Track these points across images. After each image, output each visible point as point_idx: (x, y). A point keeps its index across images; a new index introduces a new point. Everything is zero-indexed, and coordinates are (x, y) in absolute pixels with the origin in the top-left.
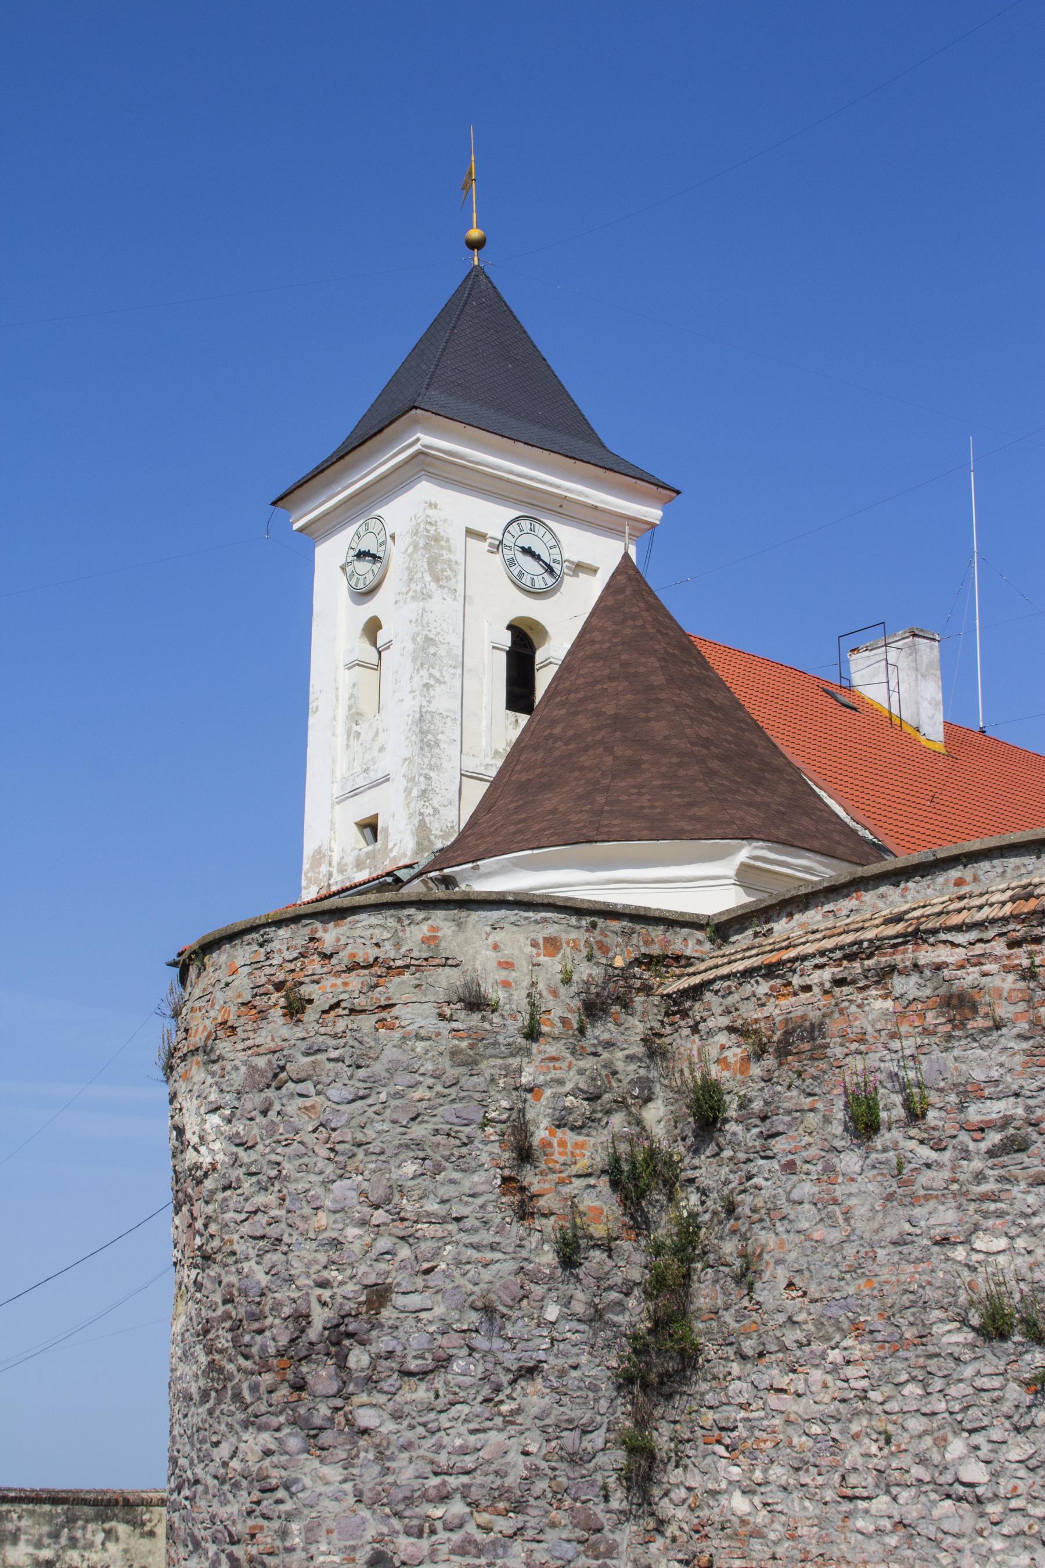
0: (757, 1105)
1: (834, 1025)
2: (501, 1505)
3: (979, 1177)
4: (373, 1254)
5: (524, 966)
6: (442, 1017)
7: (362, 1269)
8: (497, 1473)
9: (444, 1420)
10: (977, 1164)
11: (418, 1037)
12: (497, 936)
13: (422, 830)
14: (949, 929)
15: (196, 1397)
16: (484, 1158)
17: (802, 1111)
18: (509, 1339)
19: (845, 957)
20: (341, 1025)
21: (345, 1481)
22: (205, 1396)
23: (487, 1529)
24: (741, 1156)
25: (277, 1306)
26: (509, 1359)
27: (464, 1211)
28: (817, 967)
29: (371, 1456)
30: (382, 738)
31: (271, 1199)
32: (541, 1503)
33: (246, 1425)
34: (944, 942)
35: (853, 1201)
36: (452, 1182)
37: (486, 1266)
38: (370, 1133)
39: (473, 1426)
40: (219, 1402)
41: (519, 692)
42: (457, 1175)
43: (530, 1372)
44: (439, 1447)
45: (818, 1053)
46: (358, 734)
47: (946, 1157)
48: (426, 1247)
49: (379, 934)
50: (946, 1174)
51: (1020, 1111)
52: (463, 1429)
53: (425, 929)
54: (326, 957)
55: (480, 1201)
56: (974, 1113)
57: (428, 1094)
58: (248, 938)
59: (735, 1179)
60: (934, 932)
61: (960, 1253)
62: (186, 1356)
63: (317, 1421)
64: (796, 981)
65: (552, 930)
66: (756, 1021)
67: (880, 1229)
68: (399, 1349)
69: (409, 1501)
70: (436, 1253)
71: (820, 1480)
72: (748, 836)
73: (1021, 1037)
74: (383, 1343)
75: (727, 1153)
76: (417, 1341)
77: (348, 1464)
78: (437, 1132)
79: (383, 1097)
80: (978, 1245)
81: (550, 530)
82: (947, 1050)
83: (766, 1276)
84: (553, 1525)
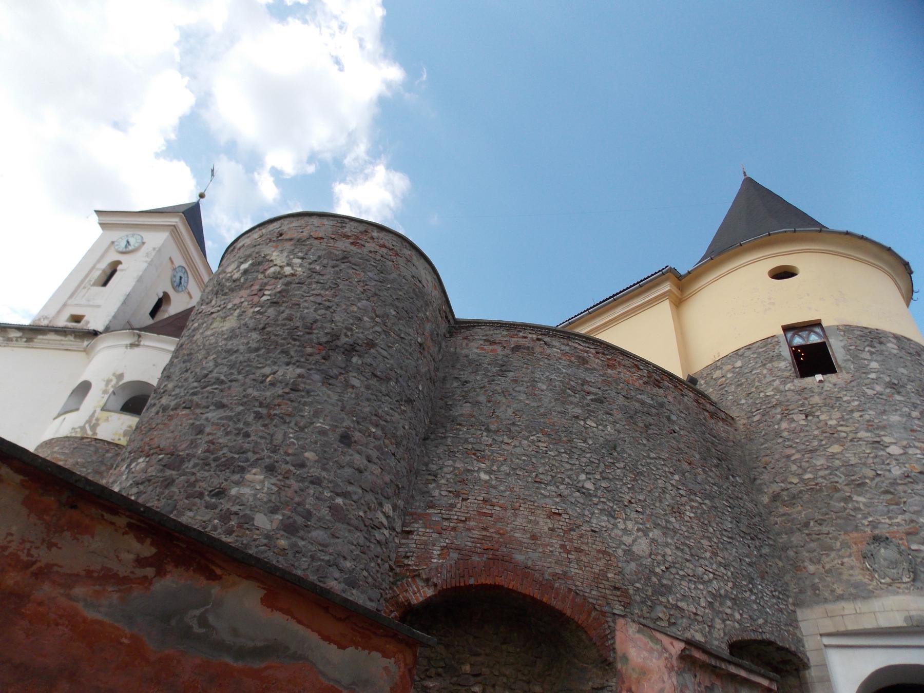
33: (288, 364)
41: (153, 313)
44: (380, 407)
49: (394, 243)
70: (394, 344)
76: (382, 366)
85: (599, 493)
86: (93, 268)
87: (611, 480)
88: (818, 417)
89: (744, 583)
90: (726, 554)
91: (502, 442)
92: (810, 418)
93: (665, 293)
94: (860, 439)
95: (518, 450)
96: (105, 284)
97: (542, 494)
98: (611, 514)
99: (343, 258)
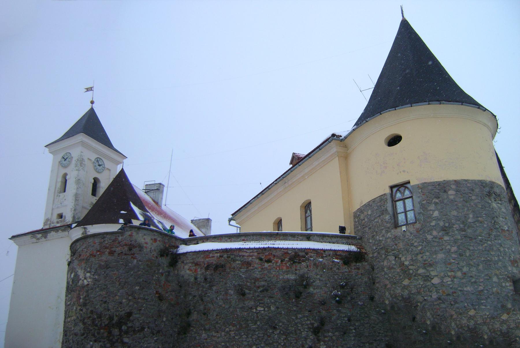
1: (228, 265)
13: (74, 217)
20: (123, 257)
24: (204, 289)
41: (94, 193)
45: (225, 271)
46: (59, 196)
58: (98, 236)
63: (114, 340)
67: (238, 305)
74: (130, 325)
76: (137, 324)
78: (143, 281)
79: (132, 273)
80: (258, 309)
83: (211, 313)
88: (400, 258)
92: (397, 259)
93: (333, 154)
94: (420, 275)
95: (220, 339)
96: (65, 191)
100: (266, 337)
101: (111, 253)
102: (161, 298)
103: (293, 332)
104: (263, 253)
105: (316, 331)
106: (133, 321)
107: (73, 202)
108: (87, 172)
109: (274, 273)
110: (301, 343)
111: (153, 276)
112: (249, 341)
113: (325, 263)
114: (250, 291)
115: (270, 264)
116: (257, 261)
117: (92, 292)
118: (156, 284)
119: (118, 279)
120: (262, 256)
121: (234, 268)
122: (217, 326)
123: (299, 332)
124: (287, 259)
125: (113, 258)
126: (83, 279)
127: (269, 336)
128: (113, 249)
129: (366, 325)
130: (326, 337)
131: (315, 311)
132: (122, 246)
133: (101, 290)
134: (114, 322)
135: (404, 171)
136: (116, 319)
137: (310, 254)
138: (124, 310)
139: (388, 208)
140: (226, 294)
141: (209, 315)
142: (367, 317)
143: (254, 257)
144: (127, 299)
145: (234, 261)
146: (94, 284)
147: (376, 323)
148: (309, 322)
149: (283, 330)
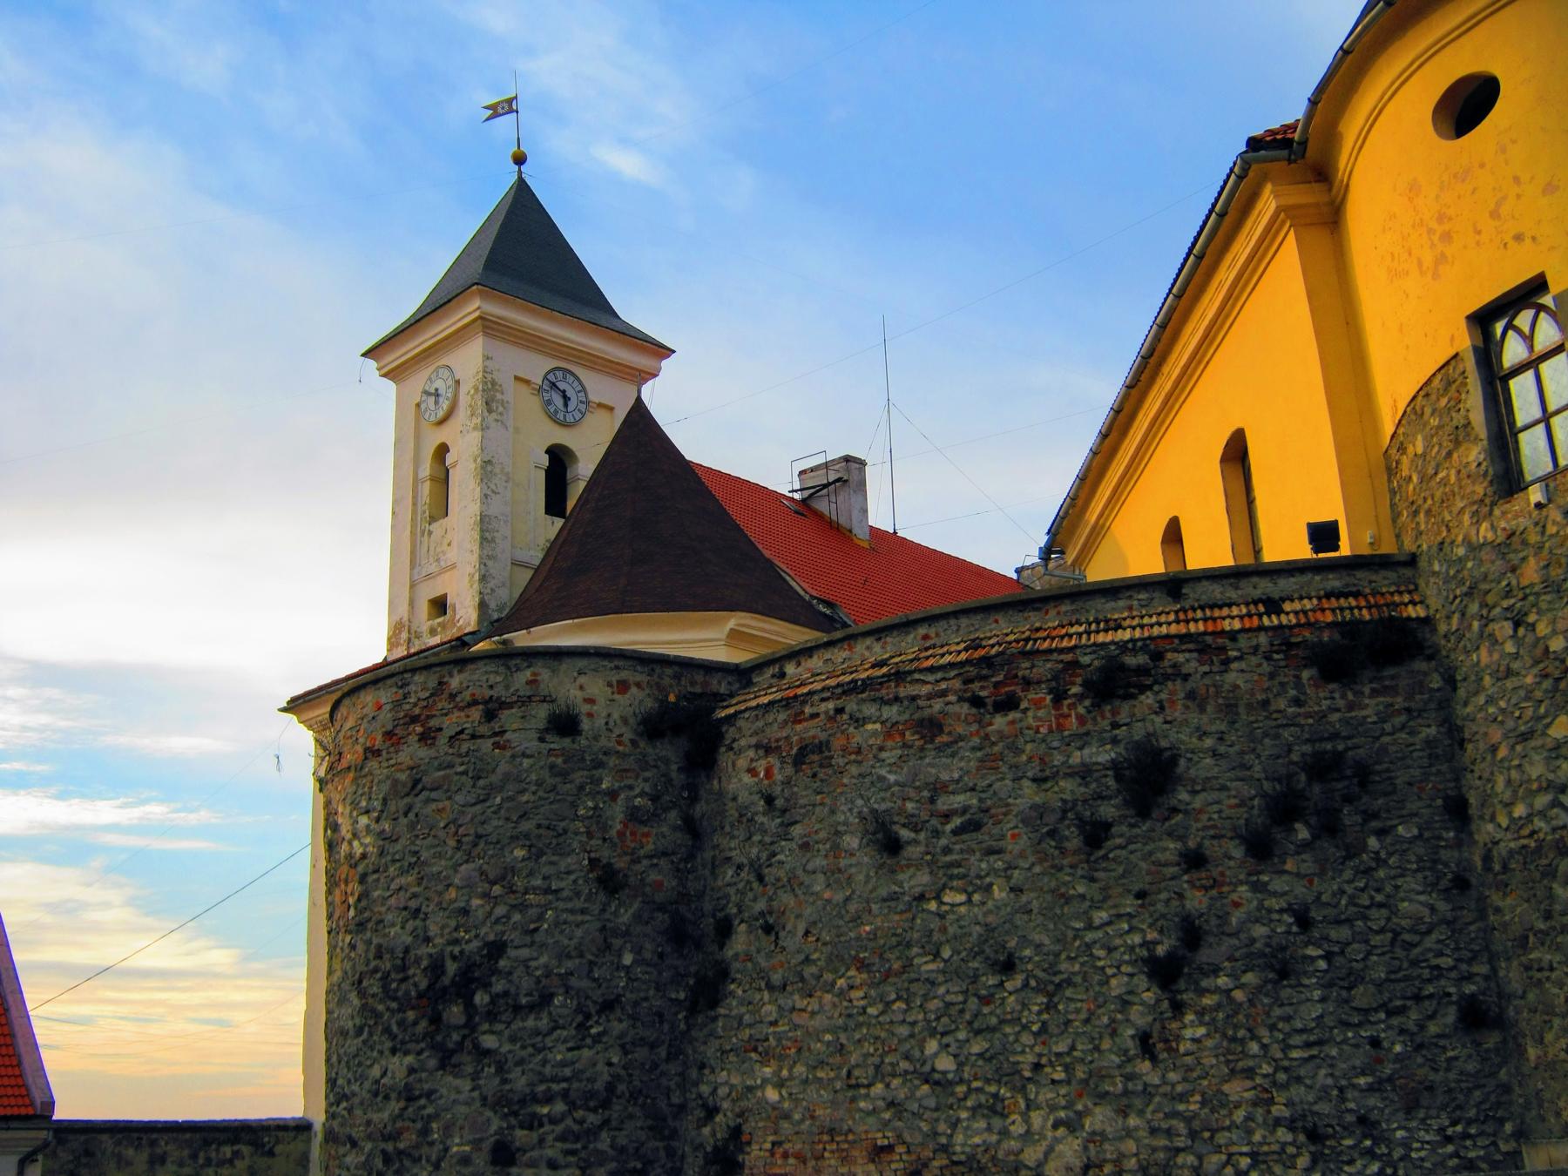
0: (779, 803)
1: (838, 742)
2: (592, 1104)
3: (947, 850)
4: (493, 918)
5: (601, 701)
6: (542, 740)
7: (483, 931)
8: (588, 1080)
9: (549, 1042)
10: (943, 842)
11: (524, 755)
12: (582, 680)
13: (483, 606)
14: (921, 671)
15: (351, 1033)
16: (575, 845)
17: (814, 805)
18: (595, 980)
19: (844, 693)
21: (473, 1090)
22: (359, 1031)
23: (581, 1122)
24: (768, 839)
25: (418, 961)
26: (597, 995)
27: (562, 884)
28: (823, 700)
29: (492, 1070)
30: (449, 536)
31: (410, 879)
32: (623, 1101)
33: (394, 1051)
34: (917, 681)
35: (853, 870)
36: (552, 863)
37: (577, 926)
38: (488, 828)
39: (570, 1045)
40: (371, 1034)
41: (555, 504)
42: (555, 858)
43: (608, 1006)
44: (545, 1062)
45: (826, 763)
47: (922, 836)
48: (533, 912)
49: (494, 679)
50: (921, 849)
51: (975, 801)
52: (563, 1048)
53: (528, 674)
54: (452, 696)
55: (573, 877)
56: (944, 803)
57: (532, 798)
58: (389, 682)
59: (764, 855)
60: (910, 672)
61: (933, 906)
62: (342, 1001)
63: (451, 1045)
64: (808, 710)
65: (624, 675)
66: (777, 741)
67: (874, 889)
68: (513, 990)
69: (523, 1102)
70: (541, 917)
71: (832, 1074)
72: (732, 608)
73: (974, 749)
74: (499, 986)
75: (756, 838)
76: (526, 983)
77: (475, 1077)
78: (539, 826)
80: (946, 899)
81: (577, 378)
82: (921, 758)
83: (789, 927)
84: (631, 1117)
85: (967, 1073)
86: (416, 481)
87: (993, 1030)
89: (1348, 1142)
90: (1297, 1092)
91: (793, 1009)
97: (861, 1110)
98: (995, 1108)
99: (413, 787)
100: (973, 1003)
101: (427, 738)
102: (609, 881)
103: (1078, 979)
104: (985, 678)
105: (1165, 973)
106: (510, 973)
107: (476, 548)
108: (517, 430)
109: (1029, 747)
110: (1105, 1020)
111: (574, 806)
112: (914, 1023)
113: (1237, 687)
114: (916, 831)
115: (1012, 715)
116: (965, 708)
117: (378, 880)
118: (590, 835)
119: (452, 829)
120: (982, 688)
121: (859, 751)
122: (810, 971)
123: (1097, 978)
124: (1075, 690)
125: (432, 753)
126: (349, 836)
127: (986, 1000)
128: (433, 723)
129: (1376, 940)
130: (1202, 992)
131: (1164, 896)
132: (462, 709)
133: (403, 872)
134: (446, 981)
135: (1519, 238)
136: (451, 968)
137: (1169, 655)
138: (477, 936)
139: (1472, 416)
140: (836, 849)
141: (782, 934)
142: (1381, 905)
143: (952, 698)
144: (486, 895)
145: (859, 722)
146: (381, 854)
147: (1423, 928)
148: (1137, 939)
149: (1041, 974)
